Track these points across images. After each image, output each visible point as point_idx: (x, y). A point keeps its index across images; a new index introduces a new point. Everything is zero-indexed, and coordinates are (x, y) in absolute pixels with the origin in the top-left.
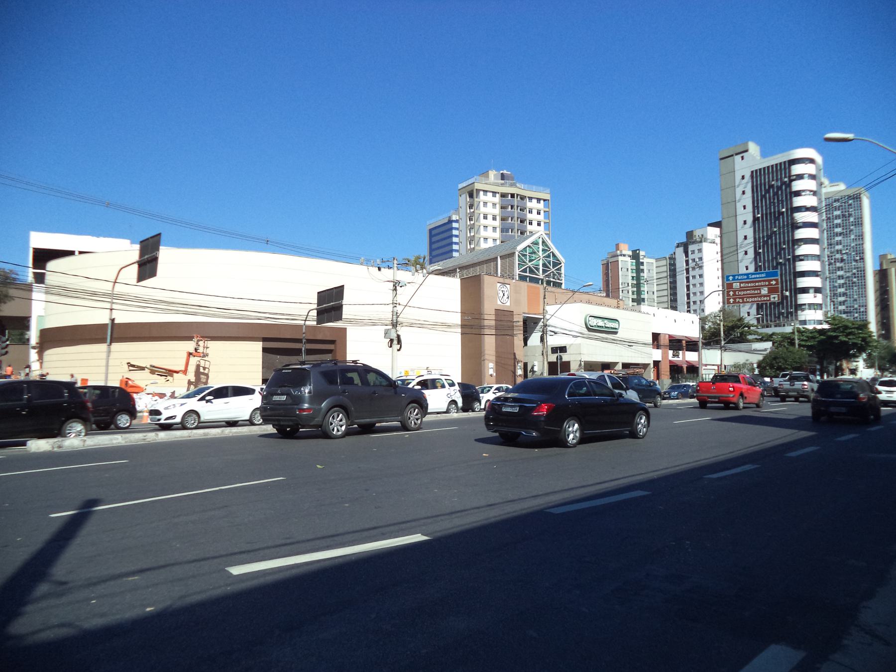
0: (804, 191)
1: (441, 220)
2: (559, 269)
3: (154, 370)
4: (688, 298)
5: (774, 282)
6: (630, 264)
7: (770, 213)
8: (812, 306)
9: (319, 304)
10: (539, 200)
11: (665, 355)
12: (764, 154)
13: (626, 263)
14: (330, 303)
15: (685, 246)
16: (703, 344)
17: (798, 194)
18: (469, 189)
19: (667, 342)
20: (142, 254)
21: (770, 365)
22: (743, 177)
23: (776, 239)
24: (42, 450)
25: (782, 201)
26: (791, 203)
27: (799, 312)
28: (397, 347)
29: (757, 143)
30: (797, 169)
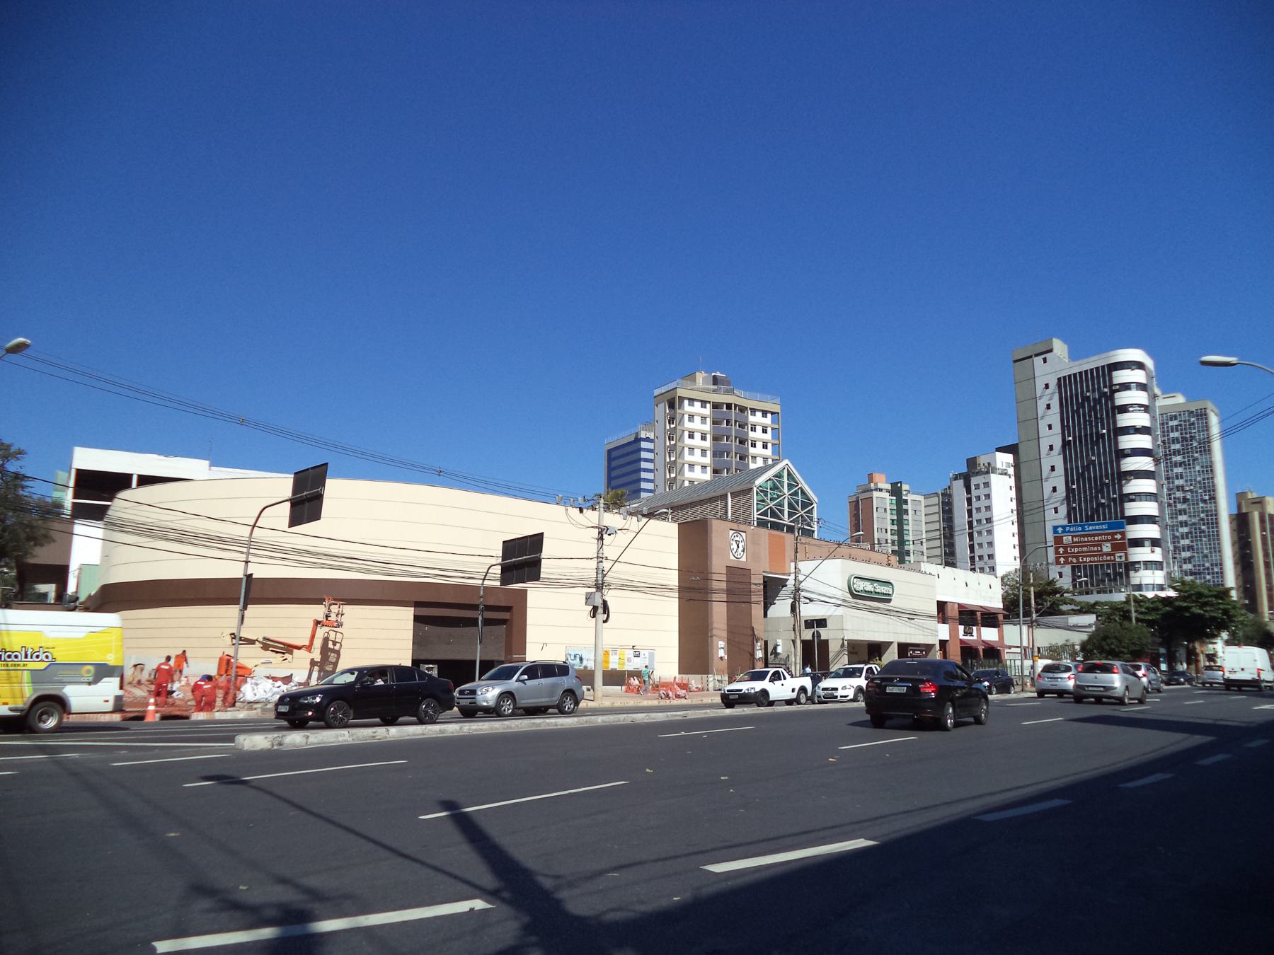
0: (1132, 405)
1: (625, 437)
2: (810, 512)
3: (267, 645)
4: (972, 550)
5: (1119, 536)
6: (888, 502)
7: (1086, 435)
8: (1149, 565)
9: (504, 558)
10: (765, 413)
11: (953, 632)
12: (1073, 356)
13: (882, 500)
14: (523, 558)
15: (966, 478)
16: (1006, 617)
17: (1124, 409)
18: (669, 396)
19: (956, 614)
20: (297, 488)
21: (1098, 651)
22: (1047, 386)
23: (1077, 467)
24: (259, 748)
25: (1102, 419)
26: (1115, 422)
27: (1132, 573)
28: (603, 617)
29: (1065, 341)
30: (1122, 376)
